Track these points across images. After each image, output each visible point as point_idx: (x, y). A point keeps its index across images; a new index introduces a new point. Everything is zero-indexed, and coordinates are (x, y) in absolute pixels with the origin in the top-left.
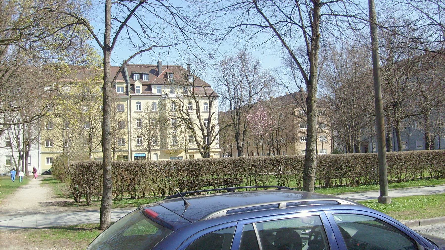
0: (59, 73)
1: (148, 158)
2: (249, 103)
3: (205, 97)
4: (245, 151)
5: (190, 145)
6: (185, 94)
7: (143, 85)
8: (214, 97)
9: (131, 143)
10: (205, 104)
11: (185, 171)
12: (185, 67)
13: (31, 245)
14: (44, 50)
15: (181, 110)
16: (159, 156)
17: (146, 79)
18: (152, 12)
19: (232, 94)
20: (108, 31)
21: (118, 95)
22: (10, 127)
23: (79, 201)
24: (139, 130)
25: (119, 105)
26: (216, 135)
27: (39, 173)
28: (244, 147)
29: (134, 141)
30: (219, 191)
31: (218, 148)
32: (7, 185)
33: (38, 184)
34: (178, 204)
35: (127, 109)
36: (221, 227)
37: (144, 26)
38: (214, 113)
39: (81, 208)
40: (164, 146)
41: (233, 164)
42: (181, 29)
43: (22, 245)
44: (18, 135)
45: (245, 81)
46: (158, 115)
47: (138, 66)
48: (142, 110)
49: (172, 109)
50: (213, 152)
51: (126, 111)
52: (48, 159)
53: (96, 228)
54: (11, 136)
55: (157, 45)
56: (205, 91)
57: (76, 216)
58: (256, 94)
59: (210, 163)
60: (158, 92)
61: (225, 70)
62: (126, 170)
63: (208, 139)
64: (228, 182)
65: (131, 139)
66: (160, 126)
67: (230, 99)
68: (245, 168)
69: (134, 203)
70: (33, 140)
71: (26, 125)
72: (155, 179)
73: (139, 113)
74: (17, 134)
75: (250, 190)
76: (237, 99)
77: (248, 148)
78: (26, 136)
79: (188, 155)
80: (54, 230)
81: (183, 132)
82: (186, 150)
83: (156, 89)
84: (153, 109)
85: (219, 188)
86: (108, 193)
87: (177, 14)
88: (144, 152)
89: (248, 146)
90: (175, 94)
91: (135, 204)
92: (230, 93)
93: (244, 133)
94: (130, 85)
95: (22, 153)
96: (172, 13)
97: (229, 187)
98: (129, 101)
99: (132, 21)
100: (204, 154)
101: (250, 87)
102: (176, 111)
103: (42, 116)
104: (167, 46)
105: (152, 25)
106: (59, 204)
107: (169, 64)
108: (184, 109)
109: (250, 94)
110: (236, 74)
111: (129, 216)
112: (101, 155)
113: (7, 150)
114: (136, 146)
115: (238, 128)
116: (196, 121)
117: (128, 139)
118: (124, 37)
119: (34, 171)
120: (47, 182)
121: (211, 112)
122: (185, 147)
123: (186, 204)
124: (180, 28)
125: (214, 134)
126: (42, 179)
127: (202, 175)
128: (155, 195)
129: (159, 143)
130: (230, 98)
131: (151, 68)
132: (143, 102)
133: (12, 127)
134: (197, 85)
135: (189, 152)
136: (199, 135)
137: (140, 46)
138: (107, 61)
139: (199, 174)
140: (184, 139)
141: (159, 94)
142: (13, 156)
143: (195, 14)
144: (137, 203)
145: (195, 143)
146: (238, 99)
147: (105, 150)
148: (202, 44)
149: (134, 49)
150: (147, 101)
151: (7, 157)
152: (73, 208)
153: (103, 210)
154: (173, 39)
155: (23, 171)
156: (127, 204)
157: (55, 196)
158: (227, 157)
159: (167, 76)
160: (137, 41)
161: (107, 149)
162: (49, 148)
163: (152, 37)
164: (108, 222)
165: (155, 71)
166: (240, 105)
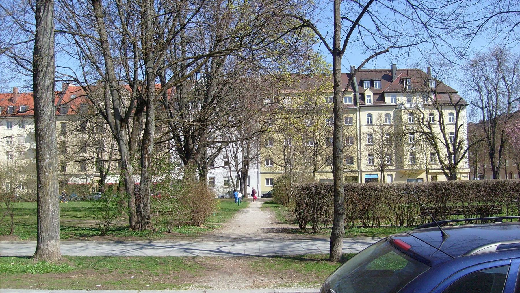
0: (281, 83)
1: (381, 179)
2: (508, 111)
3: (451, 105)
4: (502, 172)
5: (432, 164)
6: (425, 103)
7: (374, 94)
8: (462, 105)
9: (361, 162)
10: (450, 114)
11: (429, 196)
12: (425, 71)
13: (256, 275)
14: (264, 58)
15: (420, 122)
16: (394, 177)
17: (377, 86)
18: (388, 6)
19: (485, 101)
20: (337, 33)
21: (346, 107)
22: (228, 145)
23: (305, 228)
24: (370, 147)
25: (347, 118)
26: (465, 153)
27: (258, 195)
28: (501, 167)
29: (365, 159)
30: (470, 222)
31: (466, 169)
32: (226, 208)
33: (258, 208)
34: (435, 235)
35: (356, 122)
36: (490, 265)
37: (379, 23)
38: (462, 125)
39: (308, 236)
40: (400, 166)
41: (490, 188)
42: (424, 25)
43: (246, 274)
44: (236, 153)
45: (502, 84)
46: (393, 128)
47: (404, 71)
48: (373, 124)
49: (410, 121)
50: (461, 173)
51: (355, 125)
52: (268, 180)
53: (325, 259)
54: (229, 155)
55: (395, 46)
56: (450, 99)
57: (303, 245)
58: (517, 99)
59: (460, 186)
60: (392, 102)
61: (476, 71)
62: (358, 194)
63: (455, 157)
64: (482, 210)
65: (361, 157)
66: (396, 142)
67: (482, 107)
68: (506, 194)
69: (367, 232)
70: (252, 159)
71: (244, 142)
72: (392, 205)
73: (370, 127)
74: (235, 153)
75: (511, 221)
76: (491, 108)
77: (506, 168)
78: (245, 154)
79: (429, 176)
80: (279, 259)
81: (424, 149)
82: (427, 170)
83: (390, 98)
84: (386, 122)
85: (471, 218)
86: (339, 220)
87: (420, 6)
88: (376, 173)
89: (505, 166)
90: (413, 104)
91: (369, 234)
92: (482, 100)
93: (501, 149)
94: (360, 94)
95: (240, 173)
96: (413, 6)
97: (484, 218)
98: (358, 113)
99: (366, 20)
100: (449, 175)
101: (509, 91)
102: (415, 124)
103: (263, 132)
104: (406, 46)
105: (389, 21)
106: (282, 231)
107: (409, 68)
108: (424, 120)
109: (508, 101)
110: (490, 76)
111: (374, 247)
112: (331, 176)
113: (225, 170)
114: (367, 166)
115: (494, 144)
116: (440, 135)
117: (358, 158)
118: (355, 39)
119: (253, 194)
120: (268, 205)
121: (459, 123)
122: (425, 167)
123: (443, 235)
124: (423, 23)
125: (463, 151)
126: (262, 202)
127: (450, 201)
128: (392, 224)
129: (394, 162)
130: (482, 106)
131: (384, 73)
132: (375, 114)
133: (231, 144)
134: (440, 91)
135: (430, 174)
136: (443, 152)
137: (375, 48)
138: (337, 68)
139: (446, 200)
140: (425, 157)
141: (394, 104)
142: (231, 176)
143: (442, 5)
144: (371, 232)
145: (438, 162)
146: (493, 107)
147: (336, 171)
148: (450, 41)
149: (368, 52)
150: (380, 112)
151: (225, 177)
152: (298, 236)
153: (334, 239)
154: (414, 38)
155: (241, 192)
156: (359, 234)
157: (278, 221)
158: (478, 179)
159: (403, 82)
160: (370, 42)
161: (339, 169)
162: (269, 168)
163: (388, 37)
164: (339, 253)
165: (388, 76)
166: (496, 114)
